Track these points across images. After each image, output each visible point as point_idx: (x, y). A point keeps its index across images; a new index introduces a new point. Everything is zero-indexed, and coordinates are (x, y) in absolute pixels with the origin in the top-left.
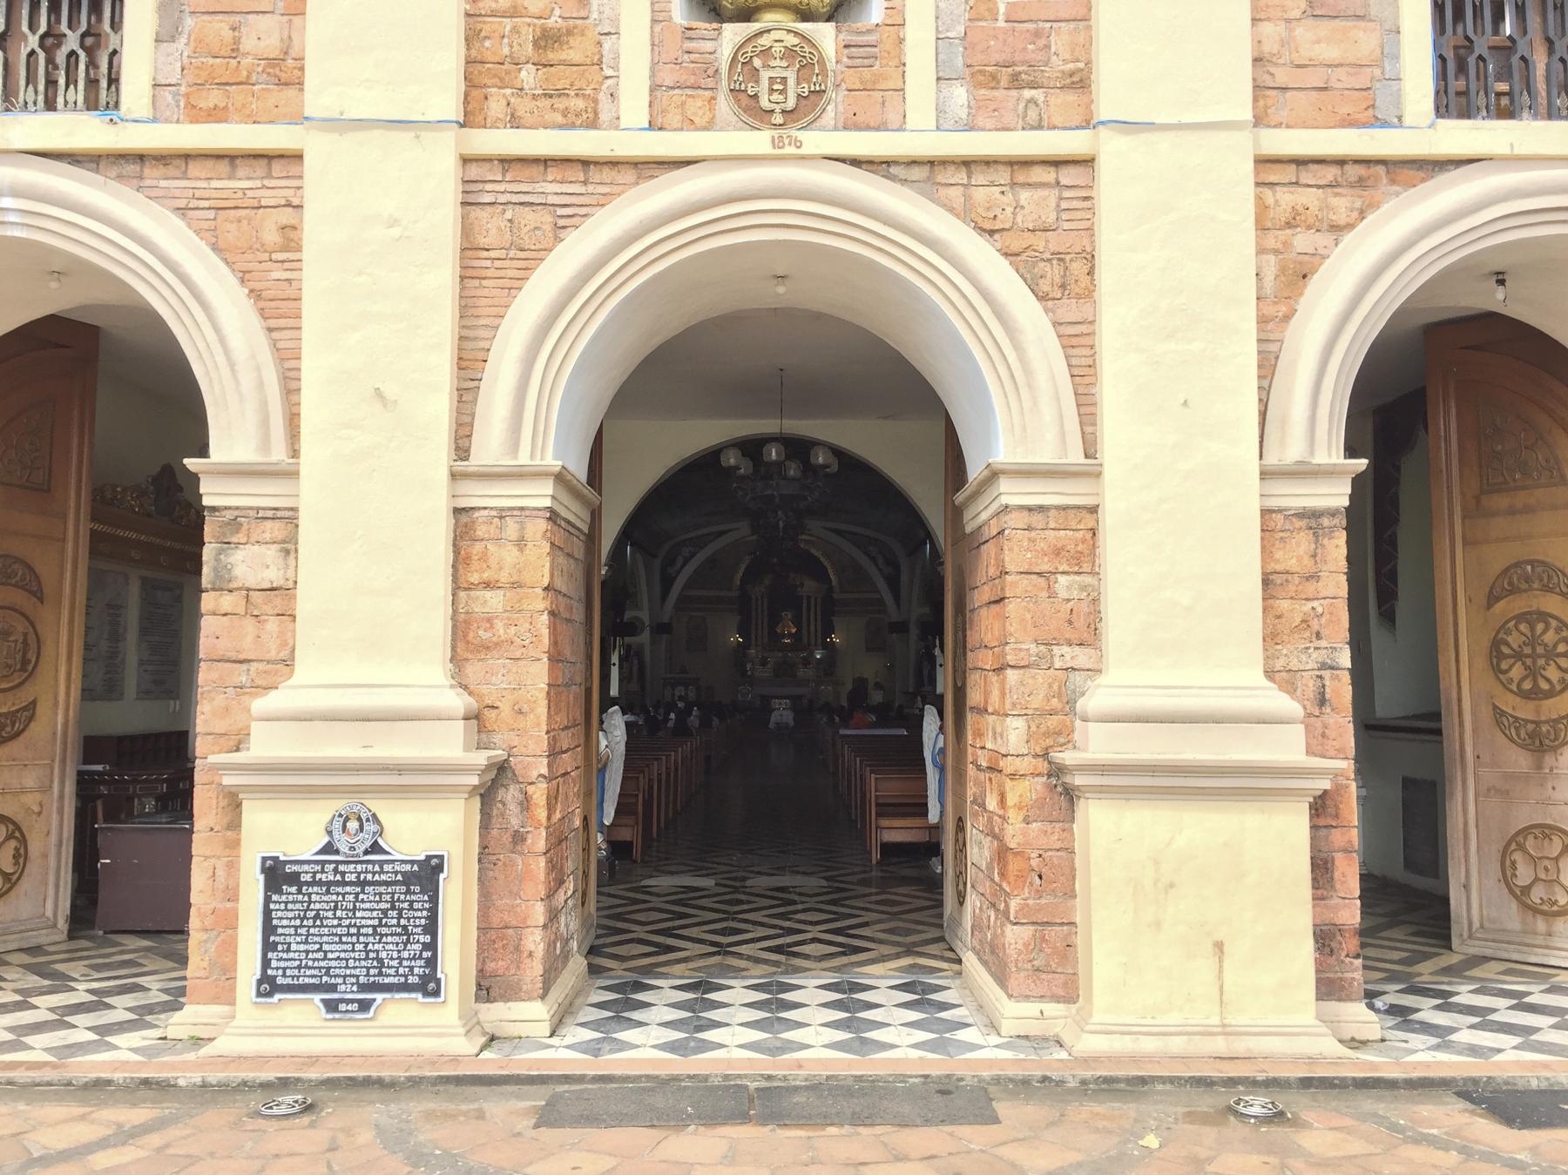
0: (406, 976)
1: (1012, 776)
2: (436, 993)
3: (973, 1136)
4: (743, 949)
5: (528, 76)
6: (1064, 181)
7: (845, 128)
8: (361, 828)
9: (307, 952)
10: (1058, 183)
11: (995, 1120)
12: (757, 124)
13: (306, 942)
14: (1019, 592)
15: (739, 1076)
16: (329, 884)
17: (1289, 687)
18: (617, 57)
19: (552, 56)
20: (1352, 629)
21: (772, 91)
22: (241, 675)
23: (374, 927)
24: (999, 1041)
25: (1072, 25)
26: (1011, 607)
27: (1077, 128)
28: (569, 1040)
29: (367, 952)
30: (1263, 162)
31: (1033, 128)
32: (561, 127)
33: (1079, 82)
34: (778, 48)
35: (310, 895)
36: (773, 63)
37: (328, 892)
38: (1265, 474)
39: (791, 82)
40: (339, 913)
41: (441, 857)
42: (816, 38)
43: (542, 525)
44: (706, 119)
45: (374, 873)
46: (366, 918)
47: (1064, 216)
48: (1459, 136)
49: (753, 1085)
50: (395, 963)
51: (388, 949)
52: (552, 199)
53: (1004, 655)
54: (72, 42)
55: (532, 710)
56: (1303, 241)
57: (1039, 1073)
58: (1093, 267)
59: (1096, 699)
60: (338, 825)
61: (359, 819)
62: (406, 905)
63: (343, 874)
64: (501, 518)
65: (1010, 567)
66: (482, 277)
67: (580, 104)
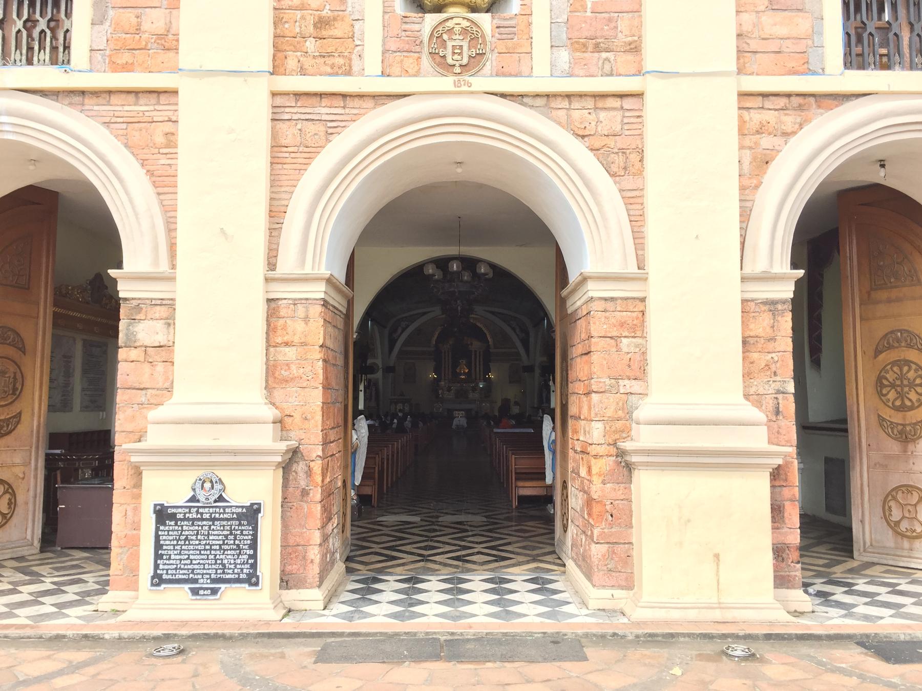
0: (239, 574)
1: (595, 457)
2: (257, 584)
3: (572, 668)
8: (213, 487)
9: (181, 560)
10: (622, 108)
11: (585, 659)
12: (445, 73)
13: (180, 554)
15: (435, 633)
16: (193, 520)
17: (758, 404)
18: (363, 34)
19: (324, 33)
20: (795, 370)
22: (142, 397)
23: (220, 545)
26: (594, 357)
27: (634, 75)
28: (334, 612)
29: (216, 560)
31: (607, 75)
32: (330, 75)
33: (635, 48)
34: (457, 28)
35: (182, 526)
36: (455, 37)
37: (193, 525)
38: (744, 279)
39: (465, 48)
40: (199, 537)
41: (259, 504)
43: (319, 309)
45: (220, 514)
46: (215, 540)
47: (626, 127)
49: (443, 638)
50: (232, 566)
51: (228, 558)
53: (590, 385)
54: (42, 24)
56: (766, 142)
57: (611, 631)
58: (642, 157)
59: (644, 411)
60: (199, 485)
61: (211, 482)
62: (239, 532)
63: (202, 514)
64: (295, 304)
65: (594, 334)
66: (284, 162)
67: (341, 61)
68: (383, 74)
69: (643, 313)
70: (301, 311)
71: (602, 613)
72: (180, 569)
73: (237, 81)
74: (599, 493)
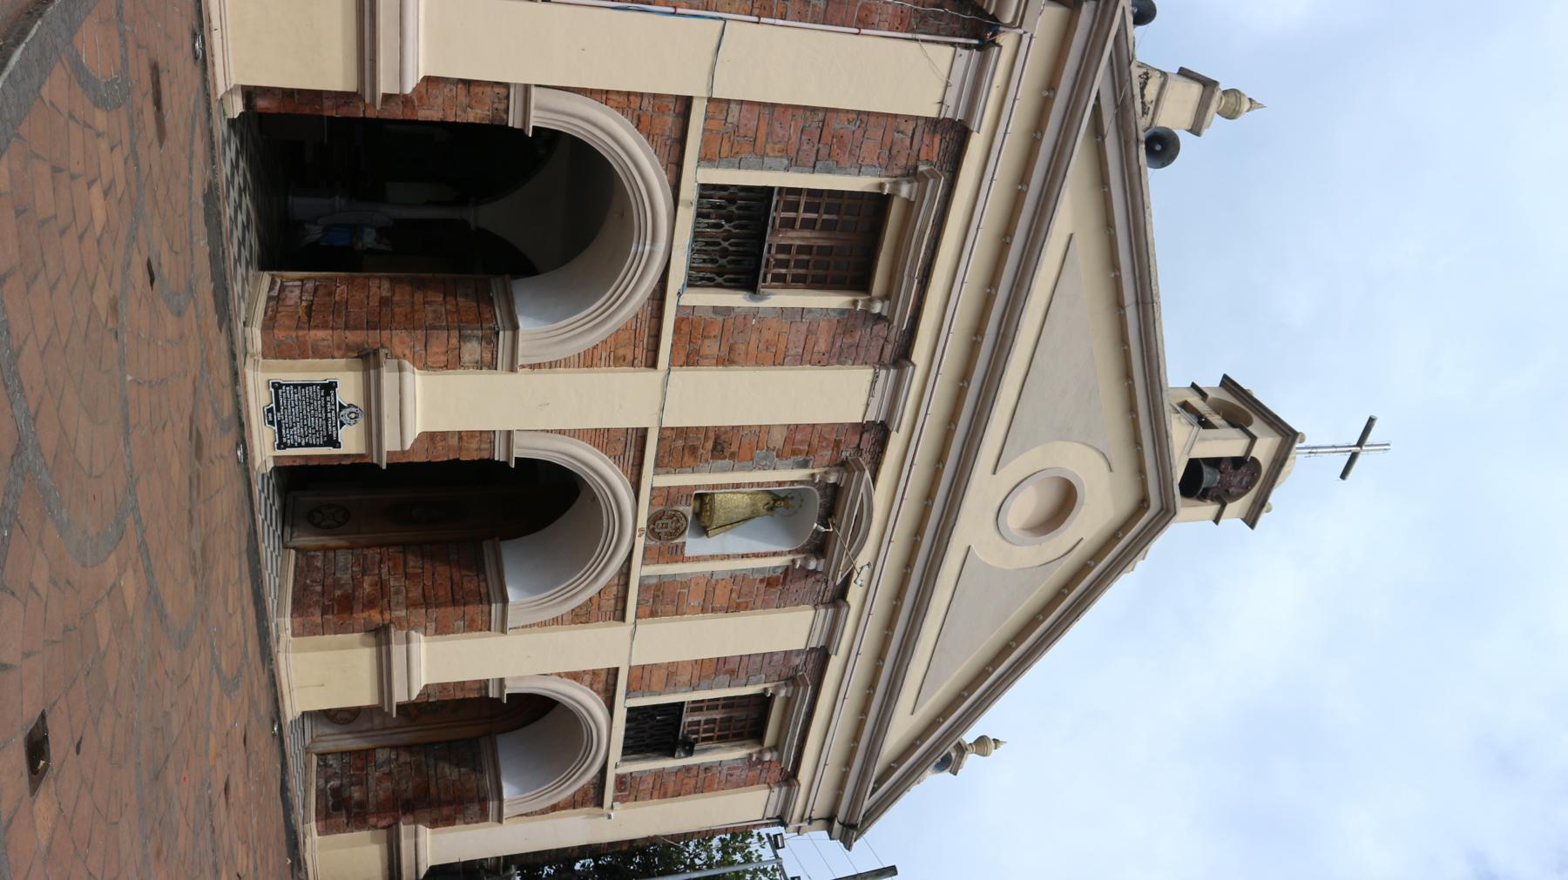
30: (687, 102)
43: (486, 455)
48: (689, 192)
54: (722, 261)
66: (626, 102)
73: (657, 409)
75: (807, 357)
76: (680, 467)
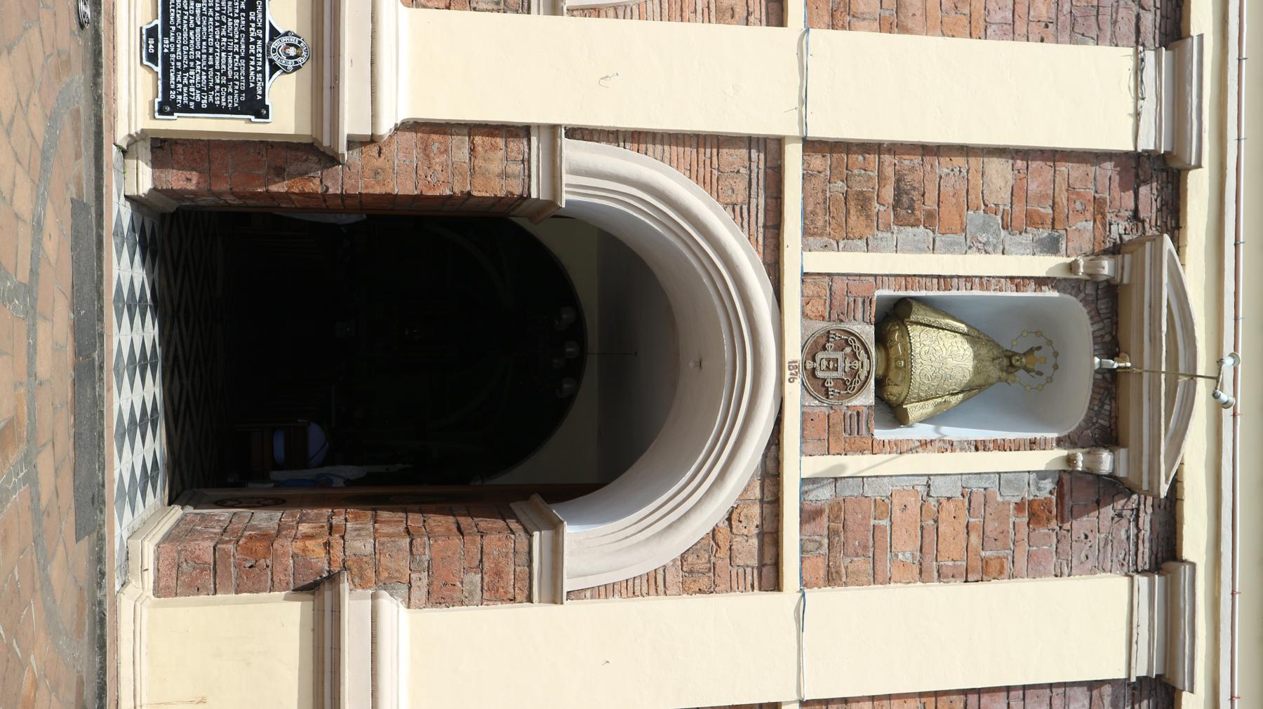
0: (175, 89)
1: (327, 545)
2: (161, 112)
3: (68, 525)
4: (176, 331)
5: (840, 186)
6: (765, 570)
7: (803, 414)
8: (290, 58)
9: (194, 15)
10: (764, 565)
11: (77, 540)
12: (806, 350)
13: (202, 15)
14: (468, 546)
15: (102, 345)
16: (247, 33)
18: (851, 250)
21: (829, 360)
23: (213, 66)
24: (125, 538)
25: (871, 572)
26: (456, 541)
27: (801, 578)
28: (123, 210)
29: (194, 60)
31: (802, 547)
32: (804, 209)
33: (832, 578)
34: (858, 364)
35: (239, 18)
36: (848, 360)
37: (241, 32)
38: (554, 128)
39: (835, 374)
40: (224, 39)
41: (267, 117)
42: (865, 392)
43: (517, 191)
44: (810, 313)
45: (255, 66)
46: (221, 60)
47: (741, 571)
49: (96, 355)
50: (185, 81)
51: (197, 76)
52: (754, 201)
53: (421, 536)
55: (378, 182)
57: (107, 570)
58: (705, 593)
59: (390, 605)
60: (293, 40)
61: (297, 56)
62: (230, 90)
63: (255, 43)
64: (523, 161)
65: (486, 539)
67: (820, 224)
68: (805, 275)
69: (513, 600)
70: (517, 168)
71: (124, 558)
72: (183, 15)
74: (280, 551)
75: (1021, 27)
76: (844, 237)
